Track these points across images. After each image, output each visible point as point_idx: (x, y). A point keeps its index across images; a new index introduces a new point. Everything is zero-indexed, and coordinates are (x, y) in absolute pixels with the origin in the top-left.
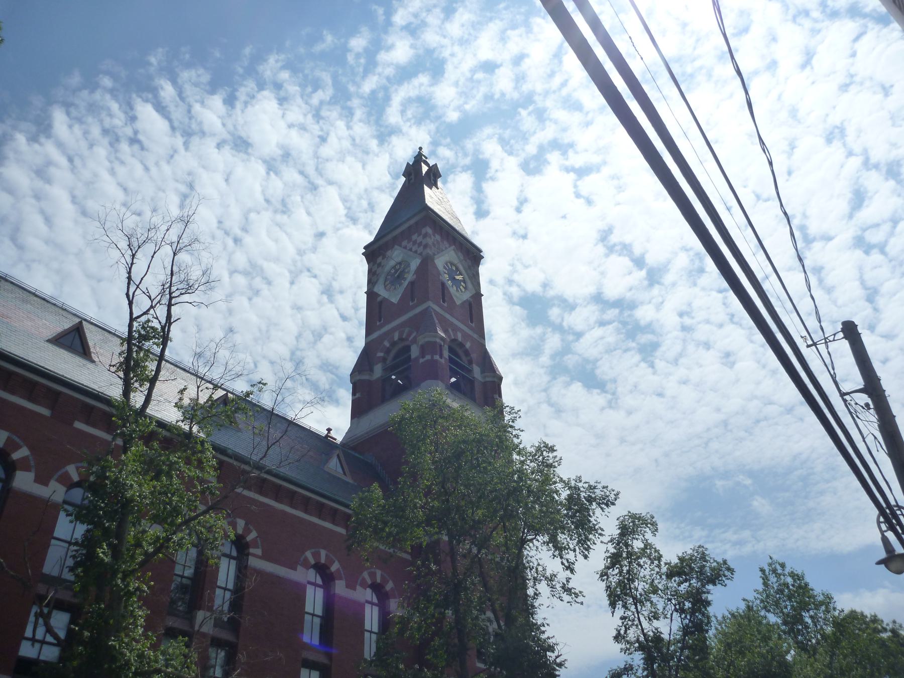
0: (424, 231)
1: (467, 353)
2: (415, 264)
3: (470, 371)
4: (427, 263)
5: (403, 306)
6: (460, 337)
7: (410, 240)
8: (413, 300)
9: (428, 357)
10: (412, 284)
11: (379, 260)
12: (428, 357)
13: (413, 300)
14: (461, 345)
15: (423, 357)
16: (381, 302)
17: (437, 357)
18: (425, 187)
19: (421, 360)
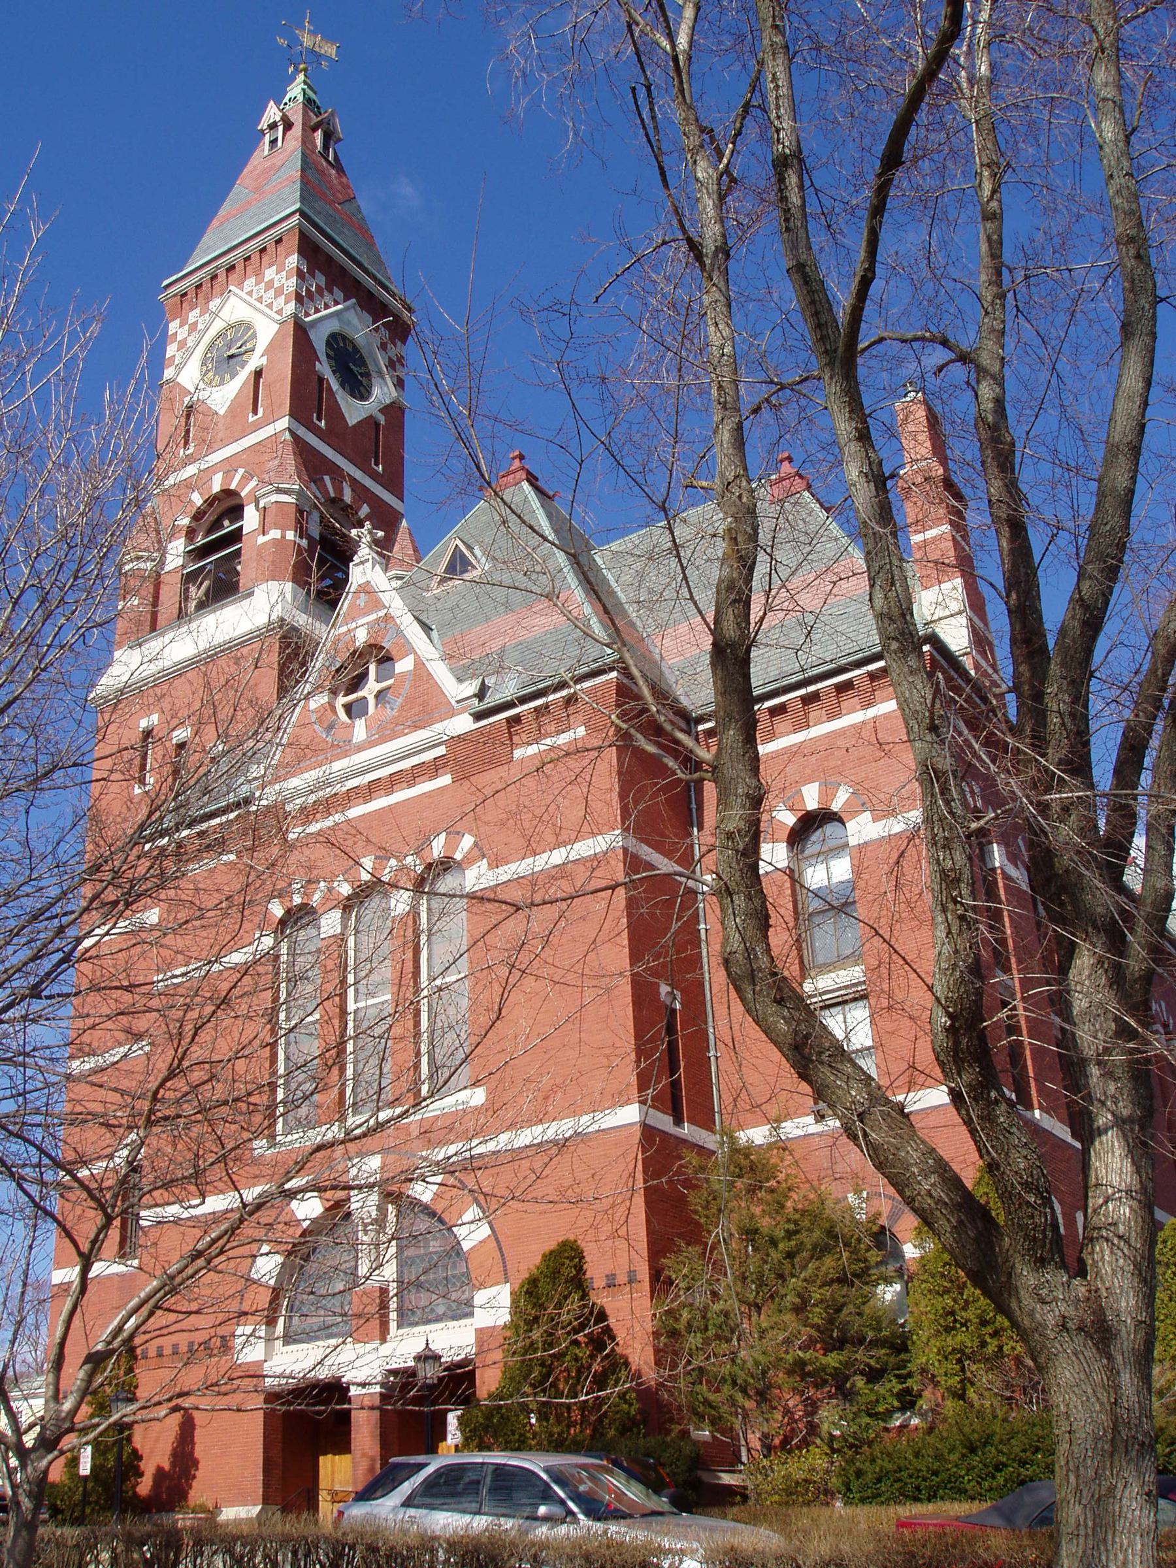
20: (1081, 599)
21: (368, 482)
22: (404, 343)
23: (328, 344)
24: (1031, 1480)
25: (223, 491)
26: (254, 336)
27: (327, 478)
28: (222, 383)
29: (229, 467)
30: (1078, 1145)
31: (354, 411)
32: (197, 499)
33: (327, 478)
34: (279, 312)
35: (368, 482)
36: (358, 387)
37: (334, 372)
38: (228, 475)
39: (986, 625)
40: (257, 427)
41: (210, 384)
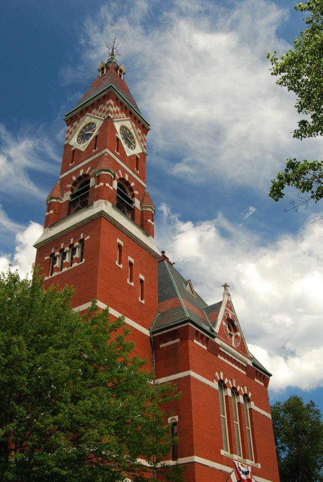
0: (108, 102)
1: (131, 189)
2: (99, 124)
3: (132, 202)
4: (108, 123)
5: (88, 152)
6: (127, 178)
7: (97, 108)
8: (72, 163)
9: (102, 184)
10: (96, 137)
11: (75, 123)
12: (102, 184)
13: (72, 163)
14: (128, 184)
15: (98, 184)
16: (74, 151)
17: (107, 185)
18: (140, 275)
19: (96, 187)
20: (229, 318)
21: (134, 176)
22: (146, 135)
23: (120, 129)
24: (135, 360)
25: (83, 175)
26: (95, 126)
27: (120, 171)
28: (84, 142)
29: (85, 167)
30: (262, 384)
31: (129, 152)
32: (74, 178)
33: (120, 171)
34: (104, 117)
35: (134, 176)
36: (131, 145)
37: (123, 139)
38: (85, 171)
39: (222, 322)
40: (95, 153)
41: (80, 143)
